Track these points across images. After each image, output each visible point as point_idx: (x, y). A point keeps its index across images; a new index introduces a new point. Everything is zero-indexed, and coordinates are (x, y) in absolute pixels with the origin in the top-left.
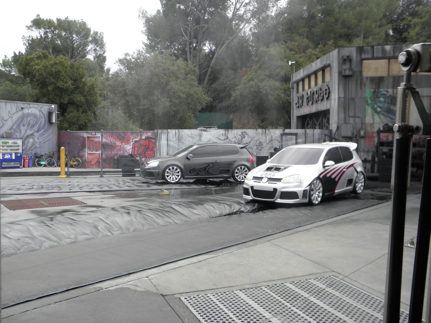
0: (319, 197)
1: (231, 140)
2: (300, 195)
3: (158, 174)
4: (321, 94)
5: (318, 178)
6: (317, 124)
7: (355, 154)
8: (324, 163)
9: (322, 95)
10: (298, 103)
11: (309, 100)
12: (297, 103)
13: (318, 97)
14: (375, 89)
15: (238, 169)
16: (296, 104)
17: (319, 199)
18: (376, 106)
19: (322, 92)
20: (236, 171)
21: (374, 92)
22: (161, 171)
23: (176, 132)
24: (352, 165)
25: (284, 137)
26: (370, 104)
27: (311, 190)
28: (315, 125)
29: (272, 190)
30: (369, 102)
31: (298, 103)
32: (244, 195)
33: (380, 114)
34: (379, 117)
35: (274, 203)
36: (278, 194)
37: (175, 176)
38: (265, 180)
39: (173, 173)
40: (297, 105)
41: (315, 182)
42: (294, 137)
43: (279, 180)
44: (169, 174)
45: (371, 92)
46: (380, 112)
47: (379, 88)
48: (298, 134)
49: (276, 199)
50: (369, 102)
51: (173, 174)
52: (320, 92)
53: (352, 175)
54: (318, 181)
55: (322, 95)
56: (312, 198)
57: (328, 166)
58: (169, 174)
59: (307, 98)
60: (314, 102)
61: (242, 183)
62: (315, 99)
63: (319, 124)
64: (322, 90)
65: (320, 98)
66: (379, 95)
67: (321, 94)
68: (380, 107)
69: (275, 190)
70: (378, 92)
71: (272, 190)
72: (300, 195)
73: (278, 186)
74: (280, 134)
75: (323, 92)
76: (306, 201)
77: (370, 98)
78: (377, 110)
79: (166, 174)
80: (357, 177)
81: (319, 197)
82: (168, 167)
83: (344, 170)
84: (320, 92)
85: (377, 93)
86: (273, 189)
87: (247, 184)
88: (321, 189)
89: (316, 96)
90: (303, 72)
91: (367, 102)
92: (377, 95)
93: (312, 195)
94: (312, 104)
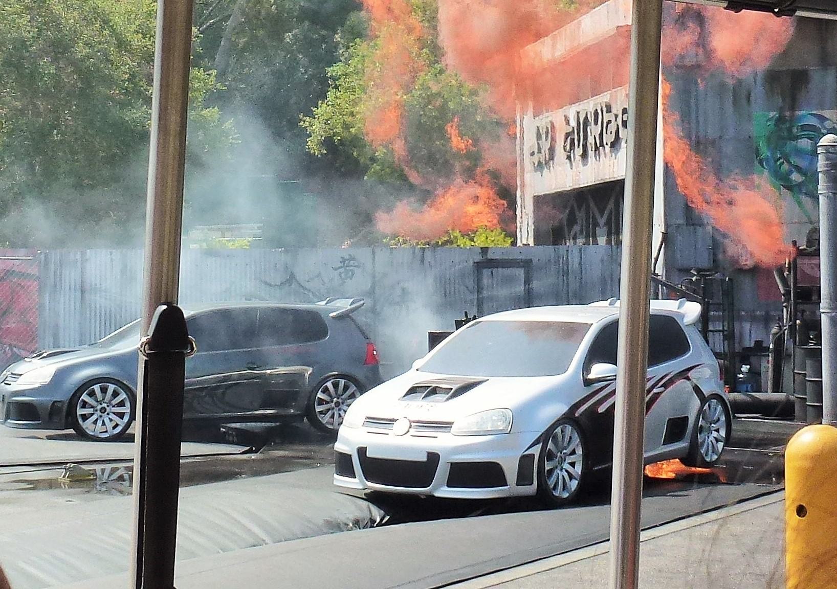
0: (717, 440)
1: (307, 285)
2: (511, 471)
3: (55, 408)
4: (609, 122)
5: (568, 418)
6: (602, 221)
7: (694, 338)
8: (586, 367)
9: (612, 127)
10: (540, 151)
11: (573, 140)
12: (536, 151)
13: (601, 134)
14: (781, 110)
15: (326, 390)
16: (532, 154)
17: (574, 485)
18: (785, 166)
19: (613, 119)
20: (320, 395)
21: (780, 120)
22: (62, 395)
23: (112, 260)
24: (684, 374)
25: (486, 272)
26: (767, 160)
27: (547, 455)
28: (596, 225)
29: (424, 458)
30: (765, 152)
31: (540, 151)
32: (336, 476)
33: (800, 191)
34: (800, 203)
35: (431, 498)
36: (442, 472)
37: (112, 416)
38: (401, 426)
39: (104, 405)
40: (536, 159)
41: (558, 430)
42: (520, 273)
43: (445, 426)
44: (91, 411)
45: (769, 120)
46: (800, 185)
47: (793, 108)
48: (535, 261)
49: (436, 489)
50: (765, 152)
51: (103, 410)
52: (607, 117)
53: (686, 405)
54: (569, 429)
55: (612, 127)
56: (551, 483)
57: (598, 380)
58: (91, 411)
59: (567, 135)
60: (591, 153)
61: (332, 436)
62: (591, 140)
63: (608, 223)
64: (614, 111)
65: (608, 138)
66: (795, 130)
67: (609, 122)
68: (799, 169)
69: (433, 458)
70: (793, 119)
71: (424, 458)
72: (511, 471)
73: (441, 443)
74: (471, 262)
75: (616, 116)
76: (531, 489)
77: (769, 140)
78: (789, 180)
79: (80, 411)
80: (701, 411)
81: (717, 440)
82: (86, 385)
83: (655, 391)
84: (607, 117)
85: (788, 125)
86: (426, 454)
87: (346, 442)
88: (579, 451)
89: (594, 130)
90: (554, 46)
91: (757, 152)
92: (790, 130)
93: (551, 472)
94: (584, 155)
